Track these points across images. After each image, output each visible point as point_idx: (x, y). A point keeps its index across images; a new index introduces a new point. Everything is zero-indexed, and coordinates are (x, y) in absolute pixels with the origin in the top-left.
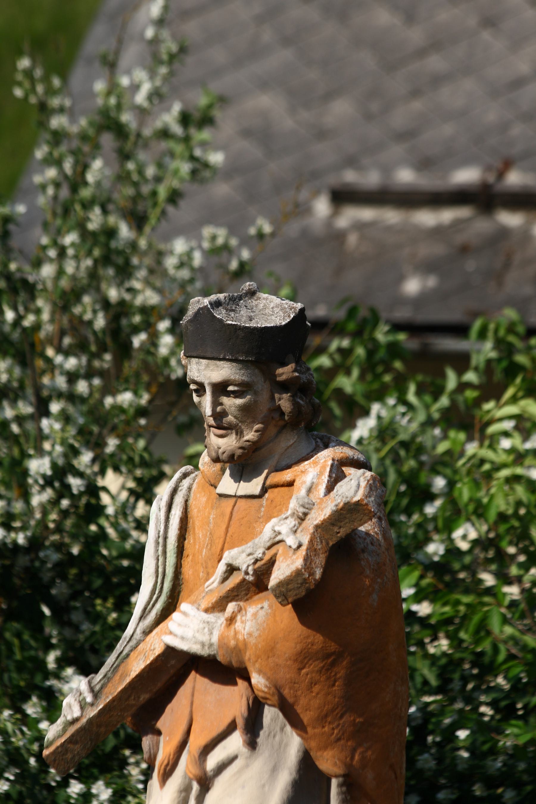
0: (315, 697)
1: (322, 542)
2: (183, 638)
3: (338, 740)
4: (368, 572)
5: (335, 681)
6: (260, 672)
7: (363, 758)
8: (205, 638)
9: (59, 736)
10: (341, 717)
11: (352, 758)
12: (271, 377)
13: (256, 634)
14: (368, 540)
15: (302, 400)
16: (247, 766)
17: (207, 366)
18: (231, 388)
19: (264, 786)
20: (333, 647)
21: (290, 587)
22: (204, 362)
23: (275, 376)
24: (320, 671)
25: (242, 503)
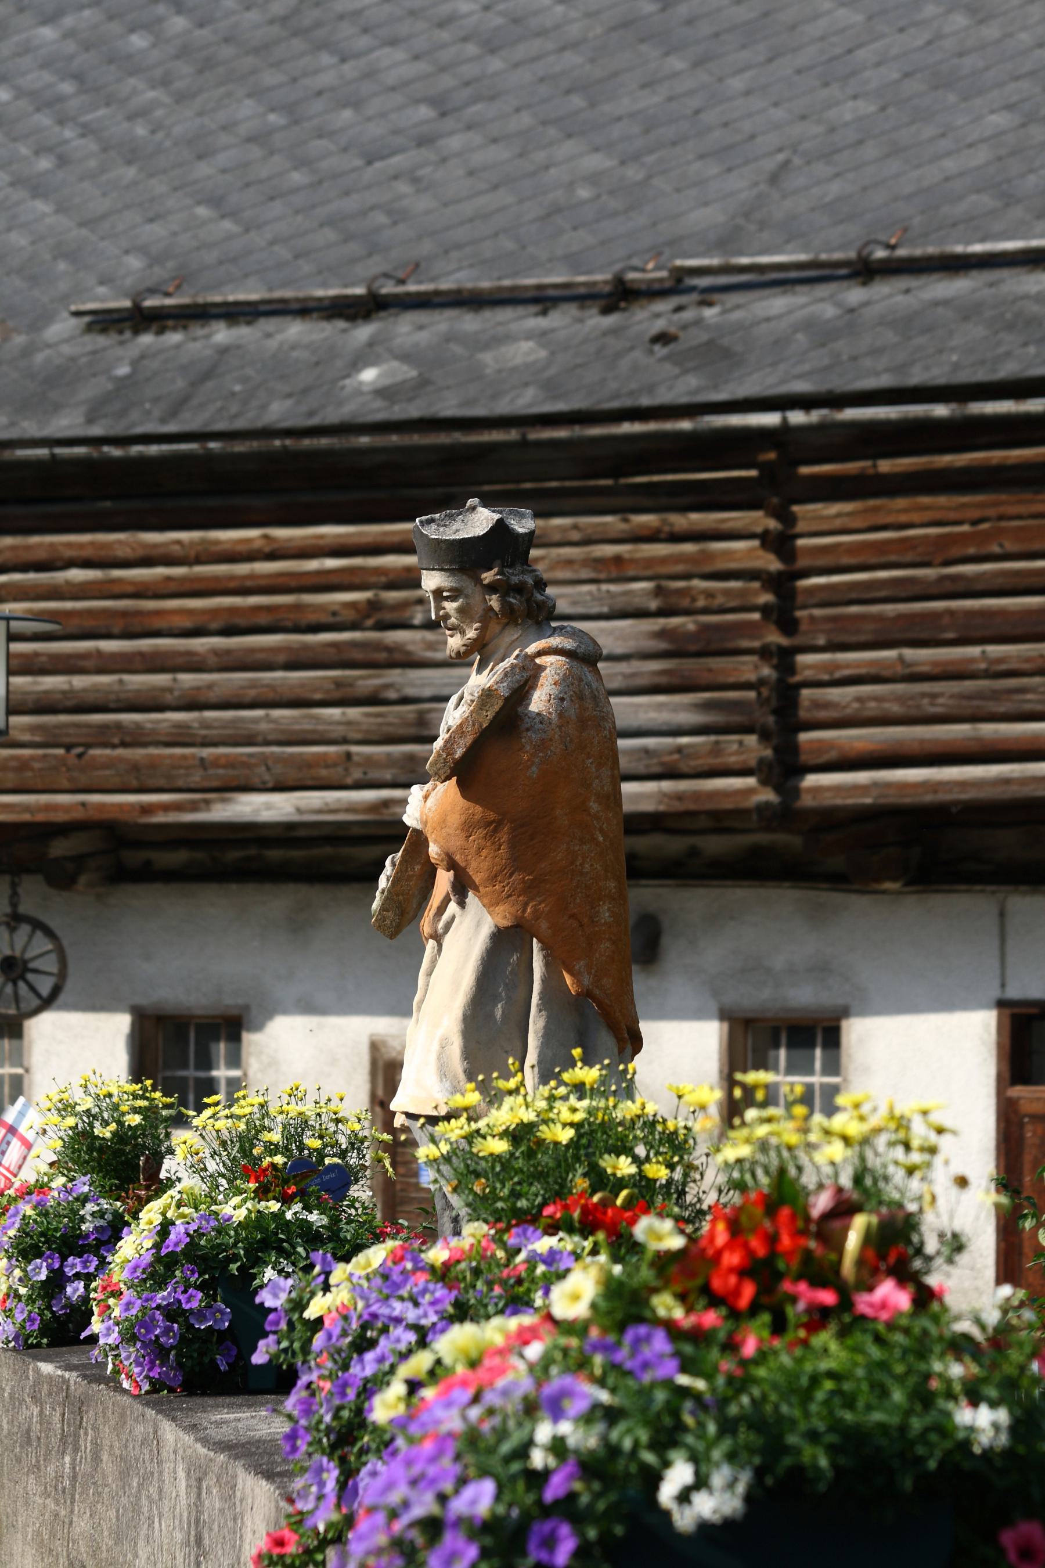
0: (484, 860)
1: (474, 725)
3: (510, 896)
4: (528, 748)
5: (500, 846)
6: (435, 841)
7: (535, 911)
10: (511, 876)
11: (524, 911)
12: (478, 581)
13: (433, 809)
14: (537, 720)
15: (514, 598)
18: (445, 594)
19: (470, 939)
20: (492, 816)
21: (438, 766)
23: (482, 580)
24: (485, 838)
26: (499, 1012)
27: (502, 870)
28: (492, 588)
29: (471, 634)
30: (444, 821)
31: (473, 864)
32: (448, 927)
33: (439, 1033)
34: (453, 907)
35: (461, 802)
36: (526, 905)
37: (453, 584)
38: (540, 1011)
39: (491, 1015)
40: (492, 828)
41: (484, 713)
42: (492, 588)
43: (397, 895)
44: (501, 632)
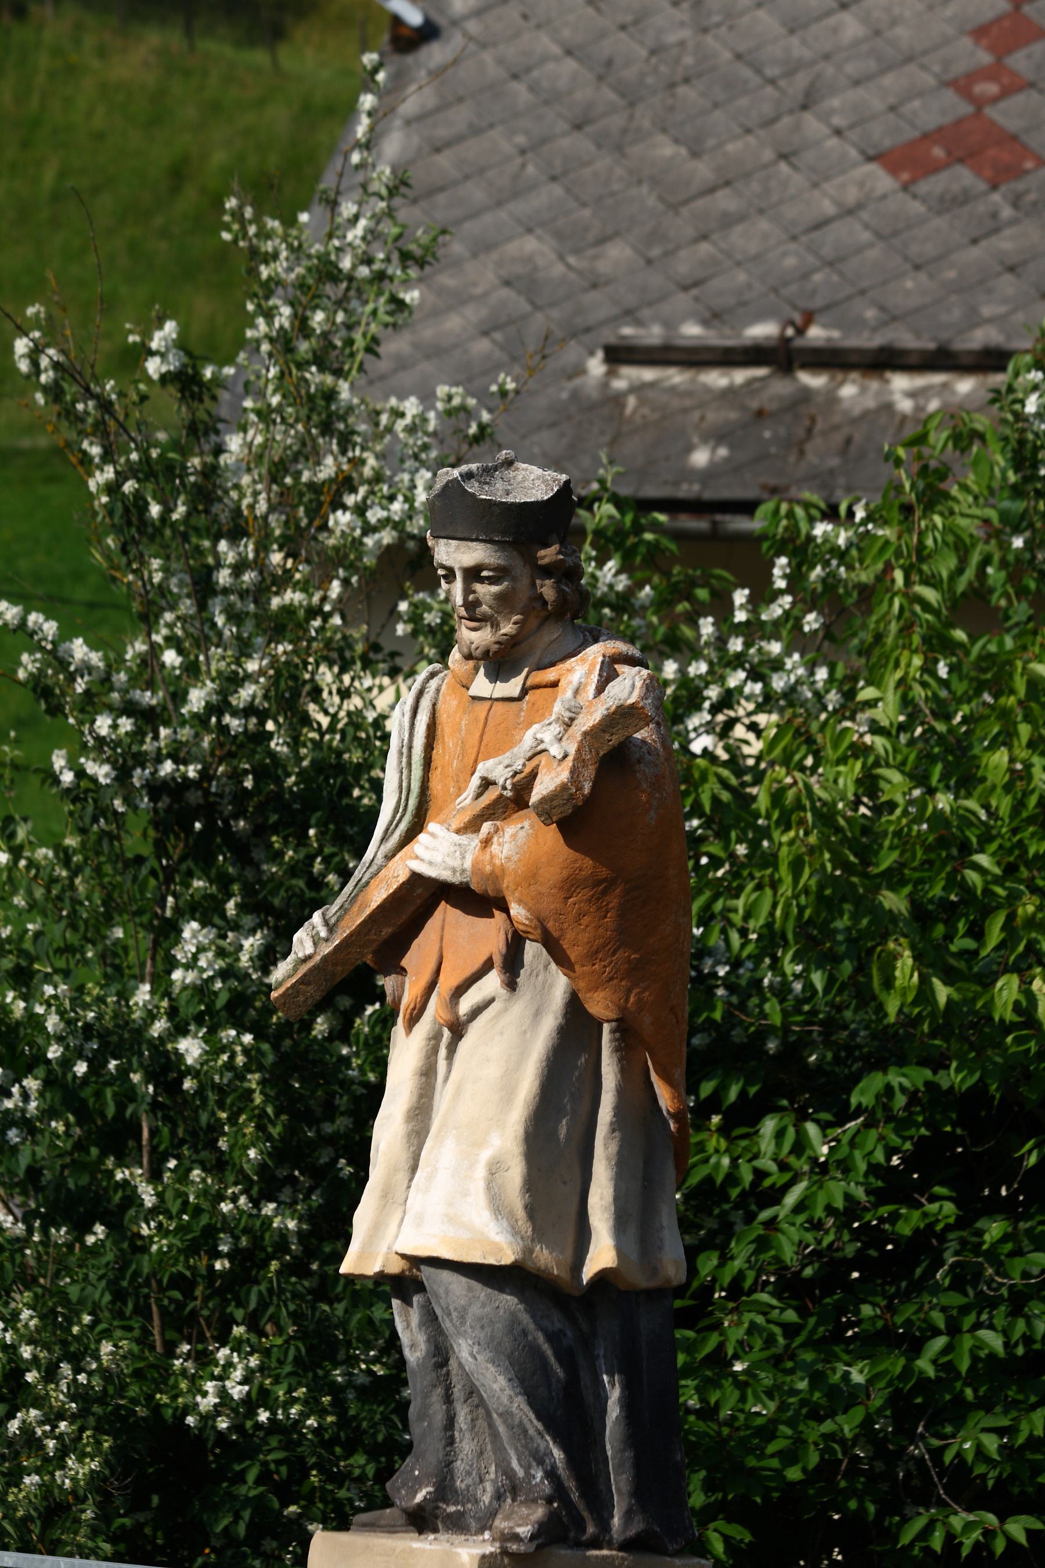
2: (430, 863)
3: (611, 979)
6: (520, 902)
7: (639, 1001)
8: (456, 863)
9: (290, 976)
10: (614, 953)
11: (627, 1000)
12: (531, 560)
13: (515, 858)
16: (506, 1010)
17: (458, 548)
18: (485, 573)
20: (604, 873)
22: (454, 543)
24: (589, 901)
25: (498, 707)
27: (604, 945)
28: (547, 571)
29: (508, 628)
31: (570, 935)
32: (476, 1012)
33: (485, 1155)
36: (629, 991)
38: (614, 1131)
40: (601, 888)
41: (607, 737)
42: (547, 571)
43: (335, 964)
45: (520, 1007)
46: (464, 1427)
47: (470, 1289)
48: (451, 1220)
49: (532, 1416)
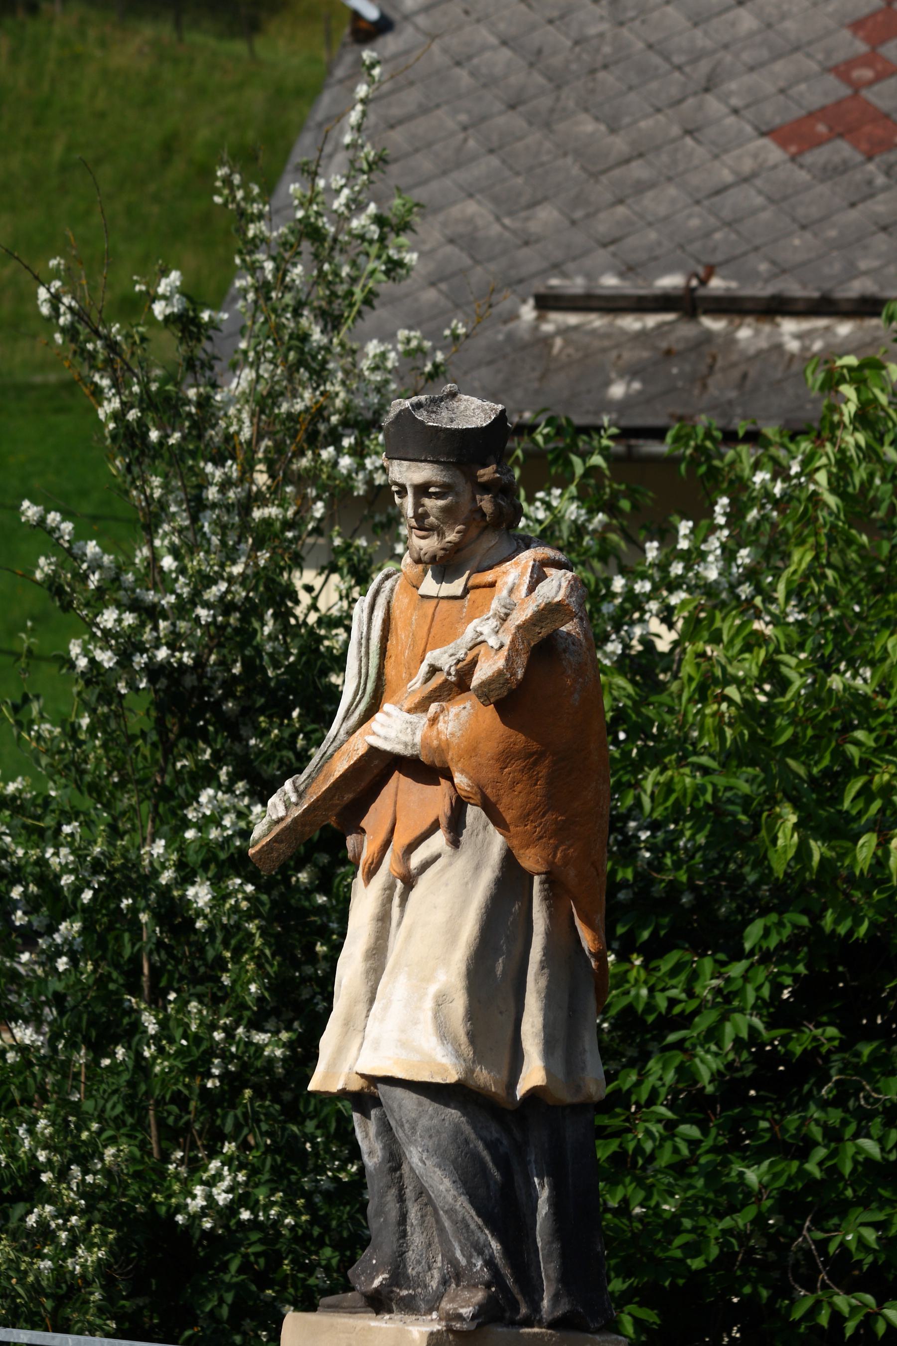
2: (386, 738)
3: (541, 838)
6: (462, 771)
7: (565, 856)
8: (408, 738)
9: (265, 836)
10: (543, 816)
11: (555, 856)
12: (472, 478)
17: (409, 468)
18: (432, 490)
20: (535, 746)
24: (522, 771)
25: (444, 604)
26: (499, 968)
27: (535, 809)
28: (485, 488)
30: (475, 749)
31: (505, 800)
32: (425, 866)
33: (433, 989)
34: (439, 841)
35: (500, 728)
36: (556, 848)
37: (445, 480)
38: (543, 968)
39: (492, 970)
40: (532, 759)
41: (537, 630)
42: (485, 488)
43: (304, 825)
44: (479, 536)
45: (463, 862)
46: (415, 1222)
47: (420, 1104)
48: (403, 1044)
49: (473, 1213)
